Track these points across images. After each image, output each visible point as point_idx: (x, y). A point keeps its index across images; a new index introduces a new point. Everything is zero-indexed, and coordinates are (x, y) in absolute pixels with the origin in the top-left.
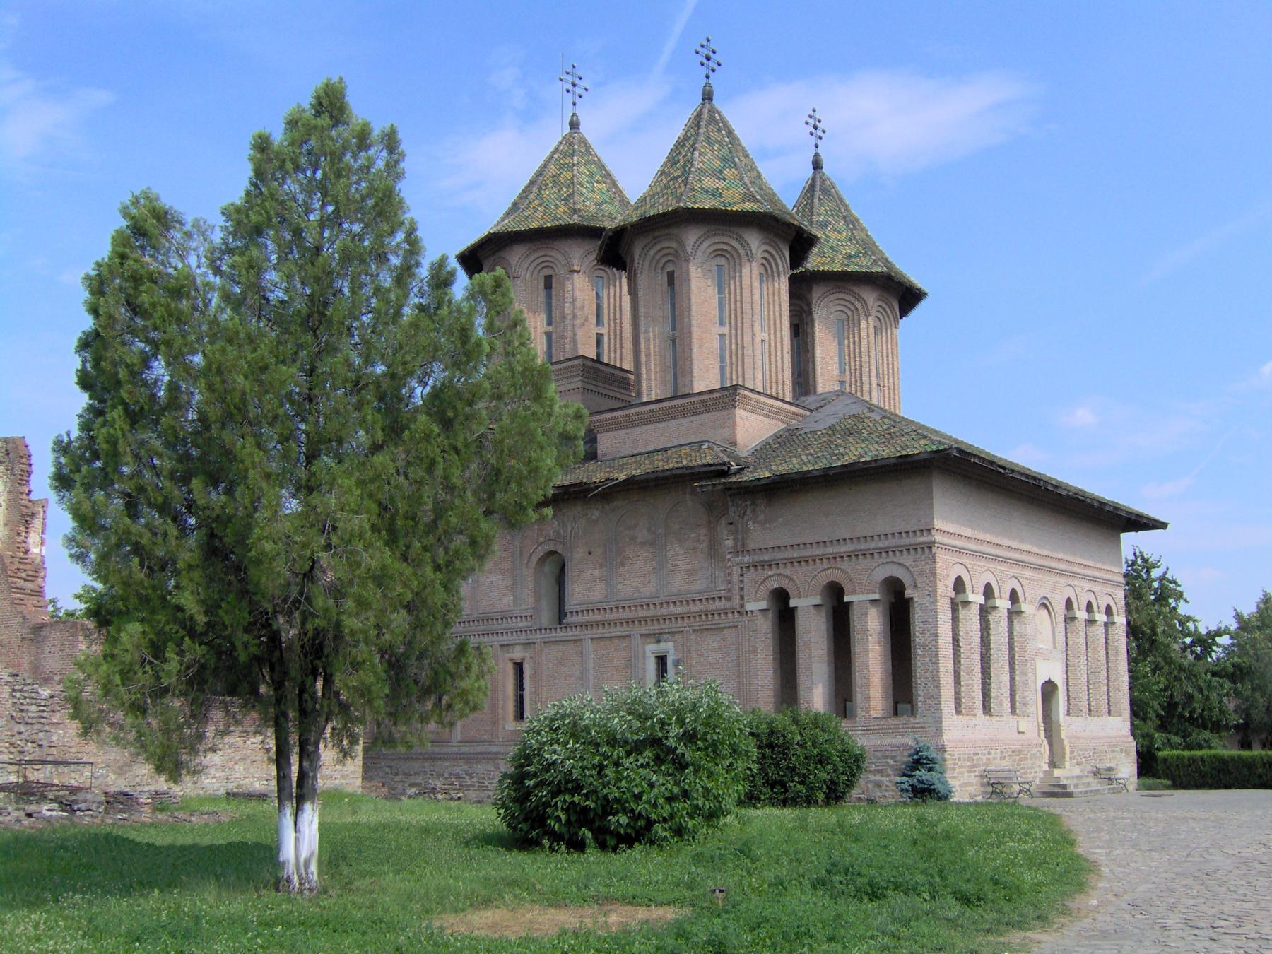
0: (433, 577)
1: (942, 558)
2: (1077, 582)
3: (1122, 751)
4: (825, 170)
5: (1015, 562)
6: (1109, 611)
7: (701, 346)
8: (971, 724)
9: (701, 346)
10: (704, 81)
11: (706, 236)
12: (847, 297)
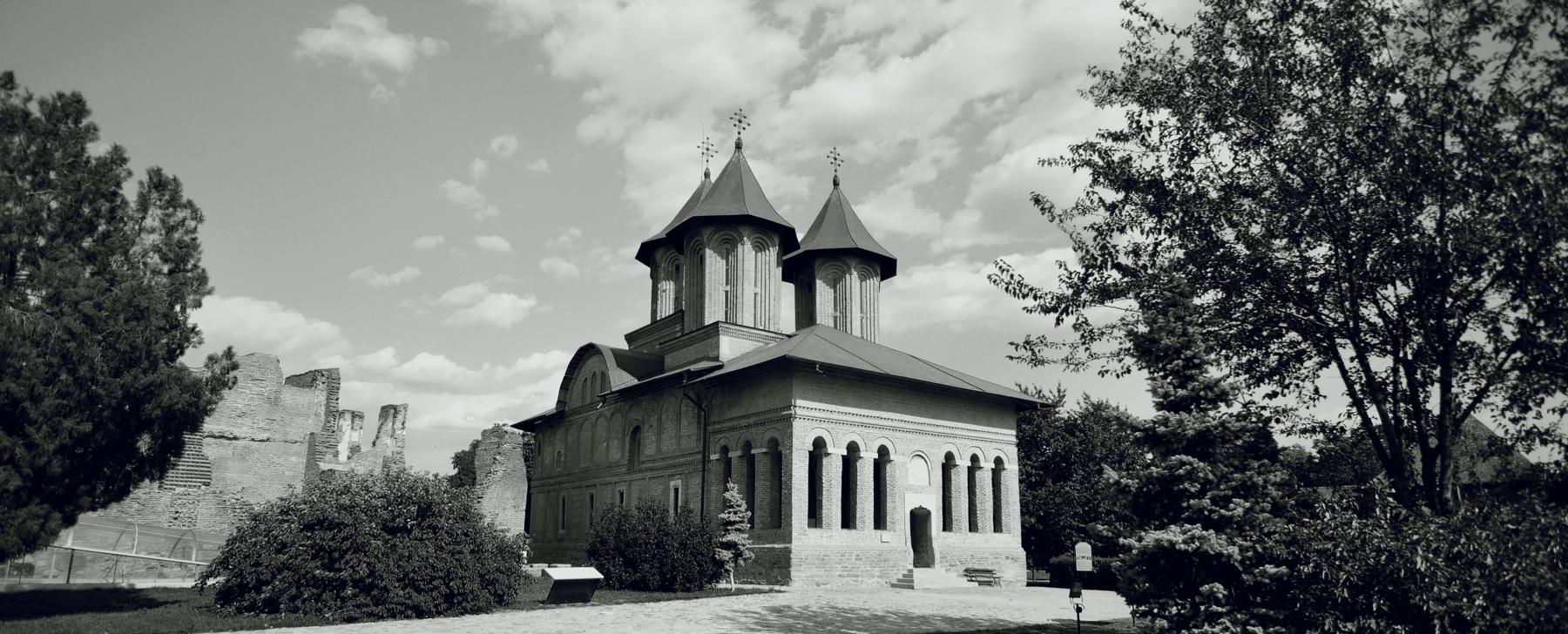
0: (1117, 477)
1: (797, 425)
2: (957, 441)
3: (1007, 558)
4: (841, 186)
5: (882, 428)
6: (998, 461)
7: (710, 299)
8: (825, 535)
9: (710, 299)
10: (737, 136)
11: (716, 232)
12: (839, 264)
